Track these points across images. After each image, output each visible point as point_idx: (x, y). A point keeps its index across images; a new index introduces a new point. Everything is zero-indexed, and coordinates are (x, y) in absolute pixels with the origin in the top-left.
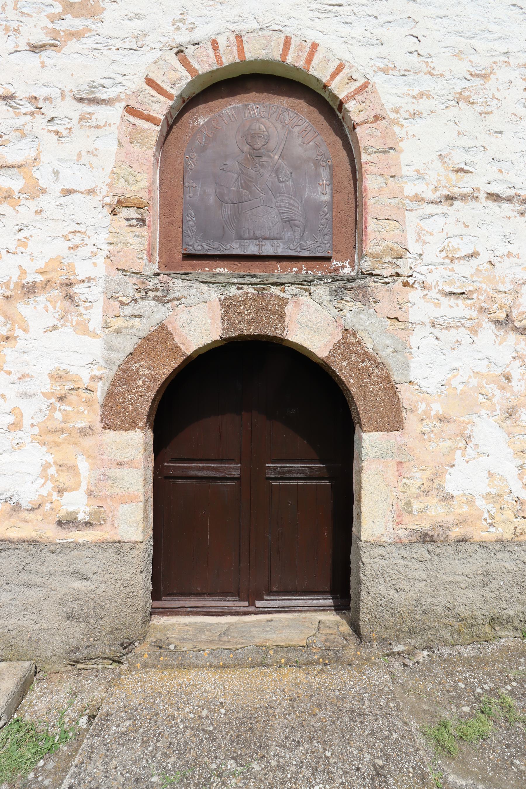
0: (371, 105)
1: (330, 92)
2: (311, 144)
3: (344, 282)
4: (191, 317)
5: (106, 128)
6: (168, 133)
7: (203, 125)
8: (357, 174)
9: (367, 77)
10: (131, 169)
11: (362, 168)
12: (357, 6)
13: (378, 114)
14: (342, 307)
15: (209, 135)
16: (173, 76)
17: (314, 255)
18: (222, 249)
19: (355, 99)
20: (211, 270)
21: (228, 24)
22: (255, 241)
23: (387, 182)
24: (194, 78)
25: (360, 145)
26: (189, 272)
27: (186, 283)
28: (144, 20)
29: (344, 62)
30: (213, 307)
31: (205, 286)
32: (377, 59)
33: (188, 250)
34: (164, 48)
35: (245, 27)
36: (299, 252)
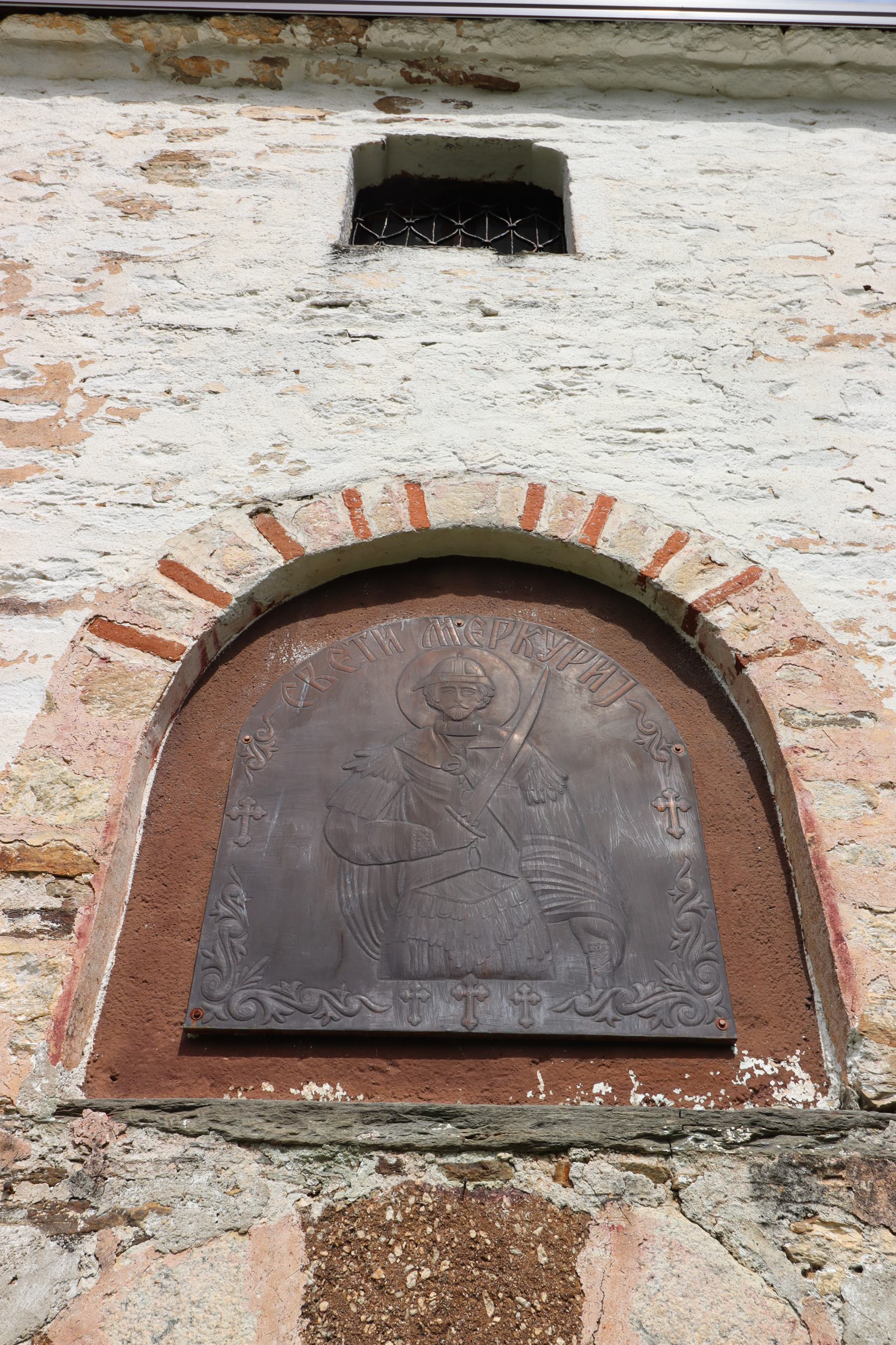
0: (777, 616)
1: (659, 589)
2: (617, 705)
3: (801, 1140)
4: (173, 1300)
5: (21, 666)
6: (201, 681)
7: (304, 663)
8: (770, 780)
9: (754, 557)
10: (65, 768)
11: (783, 763)
12: (701, 431)
13: (801, 634)
14: (817, 1254)
15: (319, 685)
16: (235, 557)
17: (670, 1033)
18: (331, 1013)
19: (729, 604)
20: (282, 1090)
21: (388, 463)
22: (451, 983)
23: (872, 799)
24: (291, 561)
25: (768, 706)
26: (196, 1100)
27: (175, 1147)
28: (183, 454)
29: (685, 530)
30: (271, 1253)
31: (249, 1156)
32: (771, 524)
33: (208, 1016)
34: (221, 504)
35: (428, 468)
36: (612, 1022)
